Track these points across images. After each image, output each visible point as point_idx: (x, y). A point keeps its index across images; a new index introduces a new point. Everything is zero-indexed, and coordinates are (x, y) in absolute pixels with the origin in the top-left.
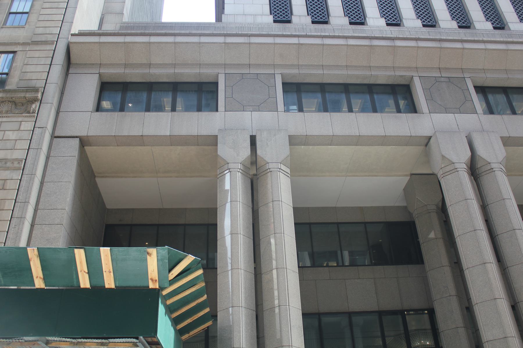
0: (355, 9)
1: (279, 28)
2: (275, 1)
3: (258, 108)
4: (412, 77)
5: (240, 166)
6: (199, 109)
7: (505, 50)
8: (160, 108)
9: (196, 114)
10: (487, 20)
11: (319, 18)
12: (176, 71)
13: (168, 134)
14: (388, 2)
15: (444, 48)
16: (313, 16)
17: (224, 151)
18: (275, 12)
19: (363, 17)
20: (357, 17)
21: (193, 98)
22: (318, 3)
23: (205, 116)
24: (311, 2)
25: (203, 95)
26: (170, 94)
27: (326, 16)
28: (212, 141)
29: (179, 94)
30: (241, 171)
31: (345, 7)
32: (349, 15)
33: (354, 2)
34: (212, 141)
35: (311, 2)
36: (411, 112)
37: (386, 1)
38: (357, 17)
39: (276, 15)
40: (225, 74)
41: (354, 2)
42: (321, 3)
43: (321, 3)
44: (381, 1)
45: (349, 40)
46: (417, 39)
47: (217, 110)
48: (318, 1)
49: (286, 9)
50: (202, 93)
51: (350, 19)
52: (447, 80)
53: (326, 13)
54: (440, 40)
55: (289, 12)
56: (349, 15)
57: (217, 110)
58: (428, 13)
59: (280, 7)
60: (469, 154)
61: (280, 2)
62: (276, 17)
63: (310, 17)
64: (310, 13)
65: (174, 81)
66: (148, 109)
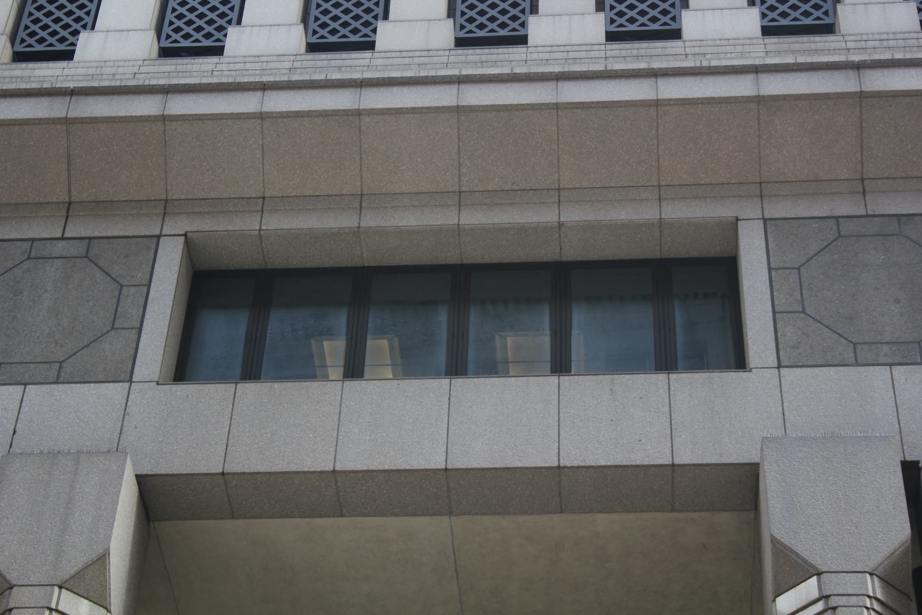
4: (734, 224)
5: (873, 587)
6: (665, 361)
7: (346, 113)
8: (304, 368)
9: (547, 385)
13: (436, 462)
15: (82, 121)
21: (639, 319)
25: (371, 316)
26: (340, 320)
28: (742, 487)
29: (373, 319)
30: (876, 606)
34: (742, 487)
36: (727, 367)
40: (765, 220)
46: (756, 70)
52: (77, 249)
54: (858, 67)
62: (774, 15)
65: (657, 255)
66: (456, 368)
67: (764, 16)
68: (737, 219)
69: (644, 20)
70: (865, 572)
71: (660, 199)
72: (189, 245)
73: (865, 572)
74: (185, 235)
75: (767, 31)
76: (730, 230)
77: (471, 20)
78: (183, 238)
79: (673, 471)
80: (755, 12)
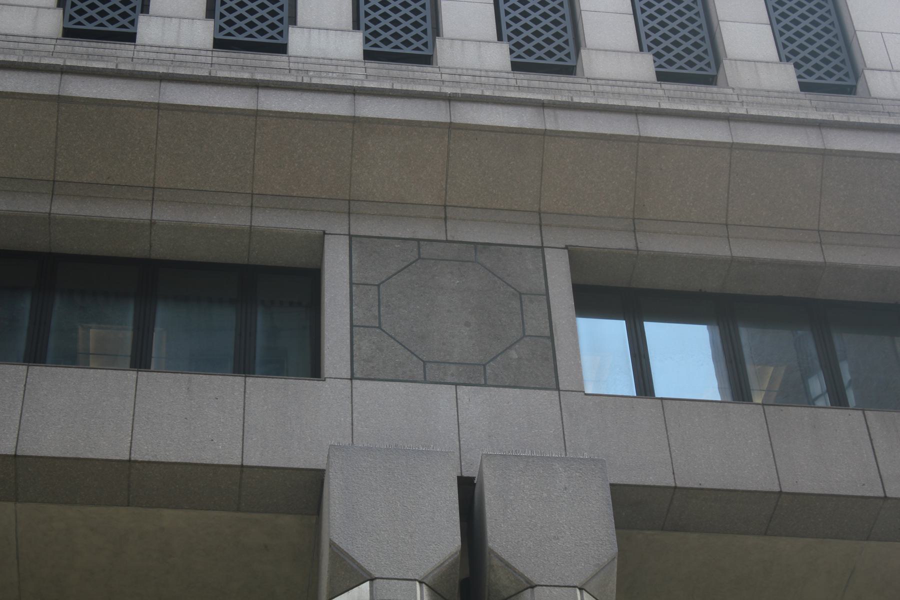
0: (683, 26)
1: (813, 108)
2: (649, 5)
3: (476, 374)
6: (243, 365)
10: (784, 58)
11: (541, 53)
12: (55, 210)
14: (811, 5)
16: (518, 45)
17: (345, 523)
18: (375, 21)
19: (709, 58)
20: (689, 58)
22: (544, 10)
23: (266, 393)
24: (375, 8)
27: (570, 48)
28: (304, 492)
31: (644, 30)
32: (658, 49)
33: (669, 6)
34: (304, 492)
35: (375, 8)
37: (801, 5)
38: (689, 58)
39: (375, 34)
40: (351, 237)
41: (669, 6)
42: (555, 10)
43: (555, 10)
44: (649, 5)
45: (362, 101)
47: (315, 371)
48: (544, 3)
49: (416, 25)
50: (261, 309)
51: (661, 61)
53: (569, 36)
55: (428, 25)
56: (657, 49)
57: (315, 371)
58: (830, 42)
59: (395, 17)
61: (263, 6)
63: (211, 23)
64: (506, 32)
67: (367, 40)
68: (324, 233)
69: (252, 31)
70: (415, 580)
71: (252, 206)
72: (576, 257)
73: (415, 580)
74: (566, 247)
75: (516, 67)
76: (317, 243)
77: (230, 23)
78: (566, 251)
79: (242, 472)
80: (505, 47)
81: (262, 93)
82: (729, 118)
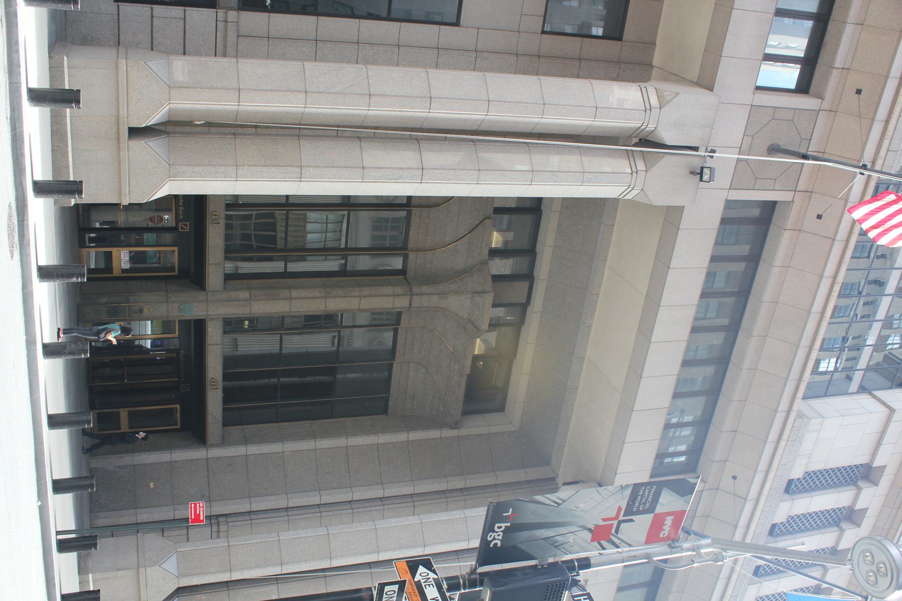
5: (651, 127)
34: (706, 82)
45: (882, 125)
60: (669, 143)
81: (796, 382)
82: (887, 122)
